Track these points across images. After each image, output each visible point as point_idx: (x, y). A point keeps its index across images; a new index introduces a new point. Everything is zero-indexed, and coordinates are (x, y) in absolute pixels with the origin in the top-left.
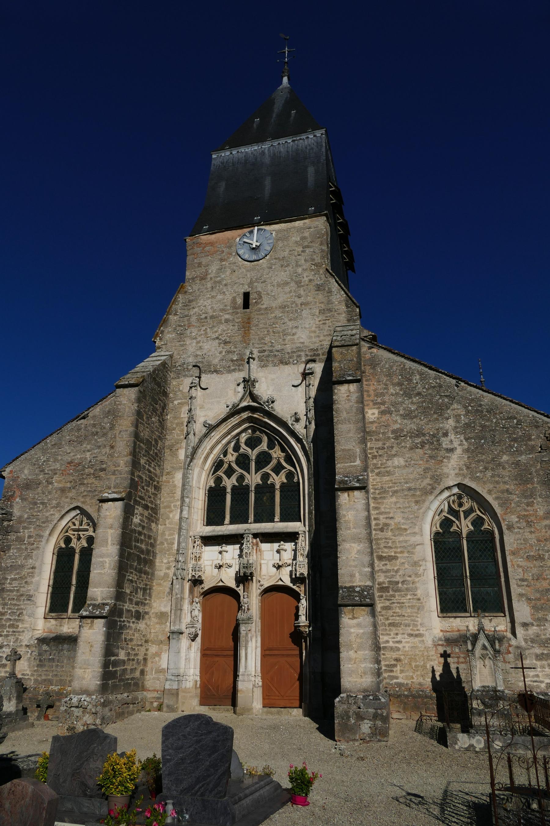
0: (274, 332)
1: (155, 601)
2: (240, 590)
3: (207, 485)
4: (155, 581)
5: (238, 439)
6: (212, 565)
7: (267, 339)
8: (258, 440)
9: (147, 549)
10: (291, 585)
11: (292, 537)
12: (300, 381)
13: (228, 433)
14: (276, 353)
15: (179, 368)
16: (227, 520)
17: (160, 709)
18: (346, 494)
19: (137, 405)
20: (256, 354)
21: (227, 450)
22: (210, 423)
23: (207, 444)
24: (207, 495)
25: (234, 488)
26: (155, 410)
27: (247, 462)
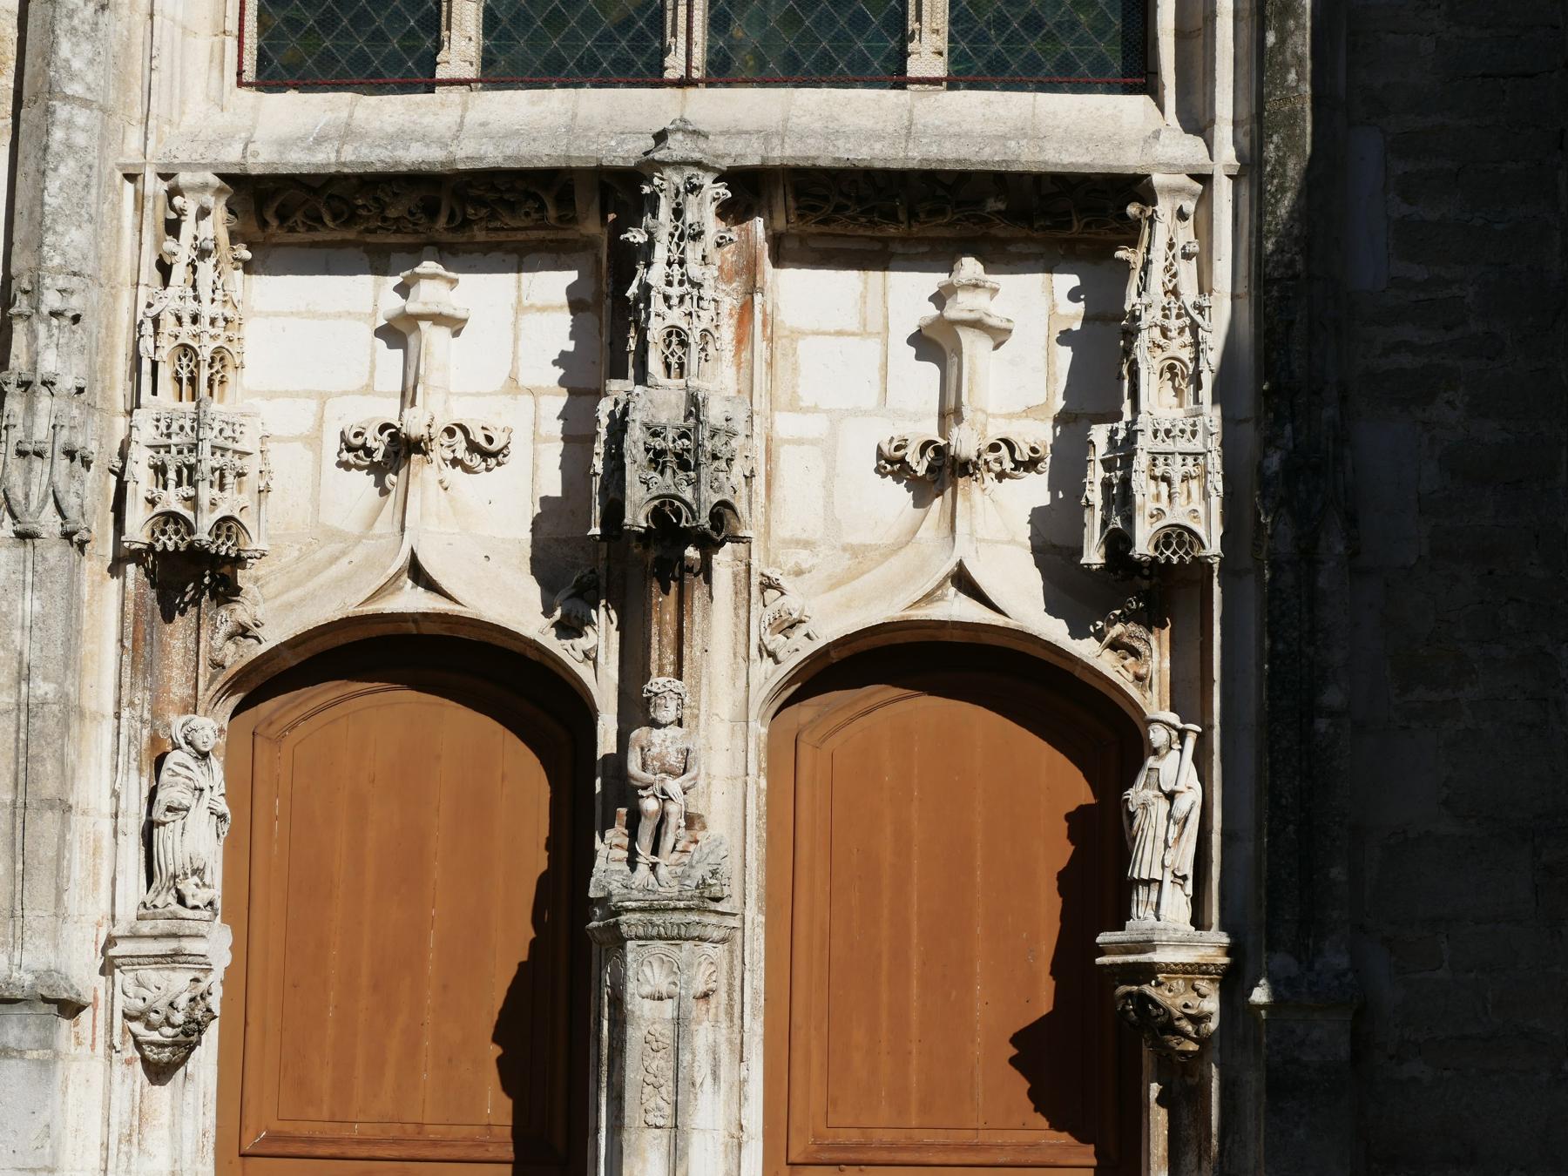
2: (595, 657)
6: (313, 441)
10: (1055, 631)
11: (1080, 220)
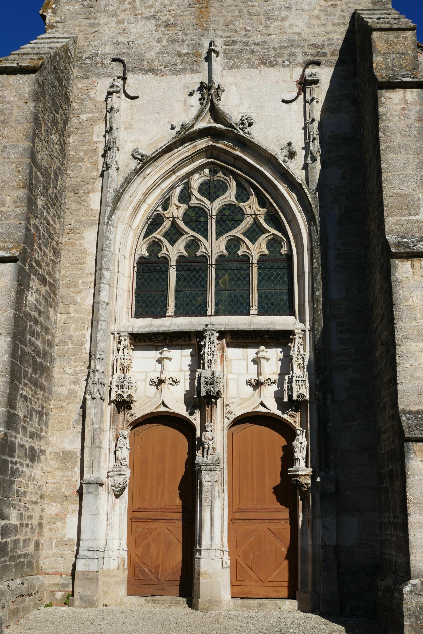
0: (250, 14)
1: (53, 434)
2: (196, 419)
3: (137, 254)
4: (53, 402)
5: (187, 184)
6: (145, 380)
7: (239, 24)
8: (221, 186)
9: (44, 350)
10: (279, 413)
11: (281, 339)
12: (295, 95)
13: (173, 171)
14: (253, 47)
15: (87, 61)
16: (171, 310)
17: (68, 601)
18: (408, 264)
19: (33, 104)
20: (219, 46)
21: (168, 199)
22: (144, 153)
23: (139, 187)
24: (136, 269)
25: (181, 259)
26: (55, 122)
27: (202, 219)
